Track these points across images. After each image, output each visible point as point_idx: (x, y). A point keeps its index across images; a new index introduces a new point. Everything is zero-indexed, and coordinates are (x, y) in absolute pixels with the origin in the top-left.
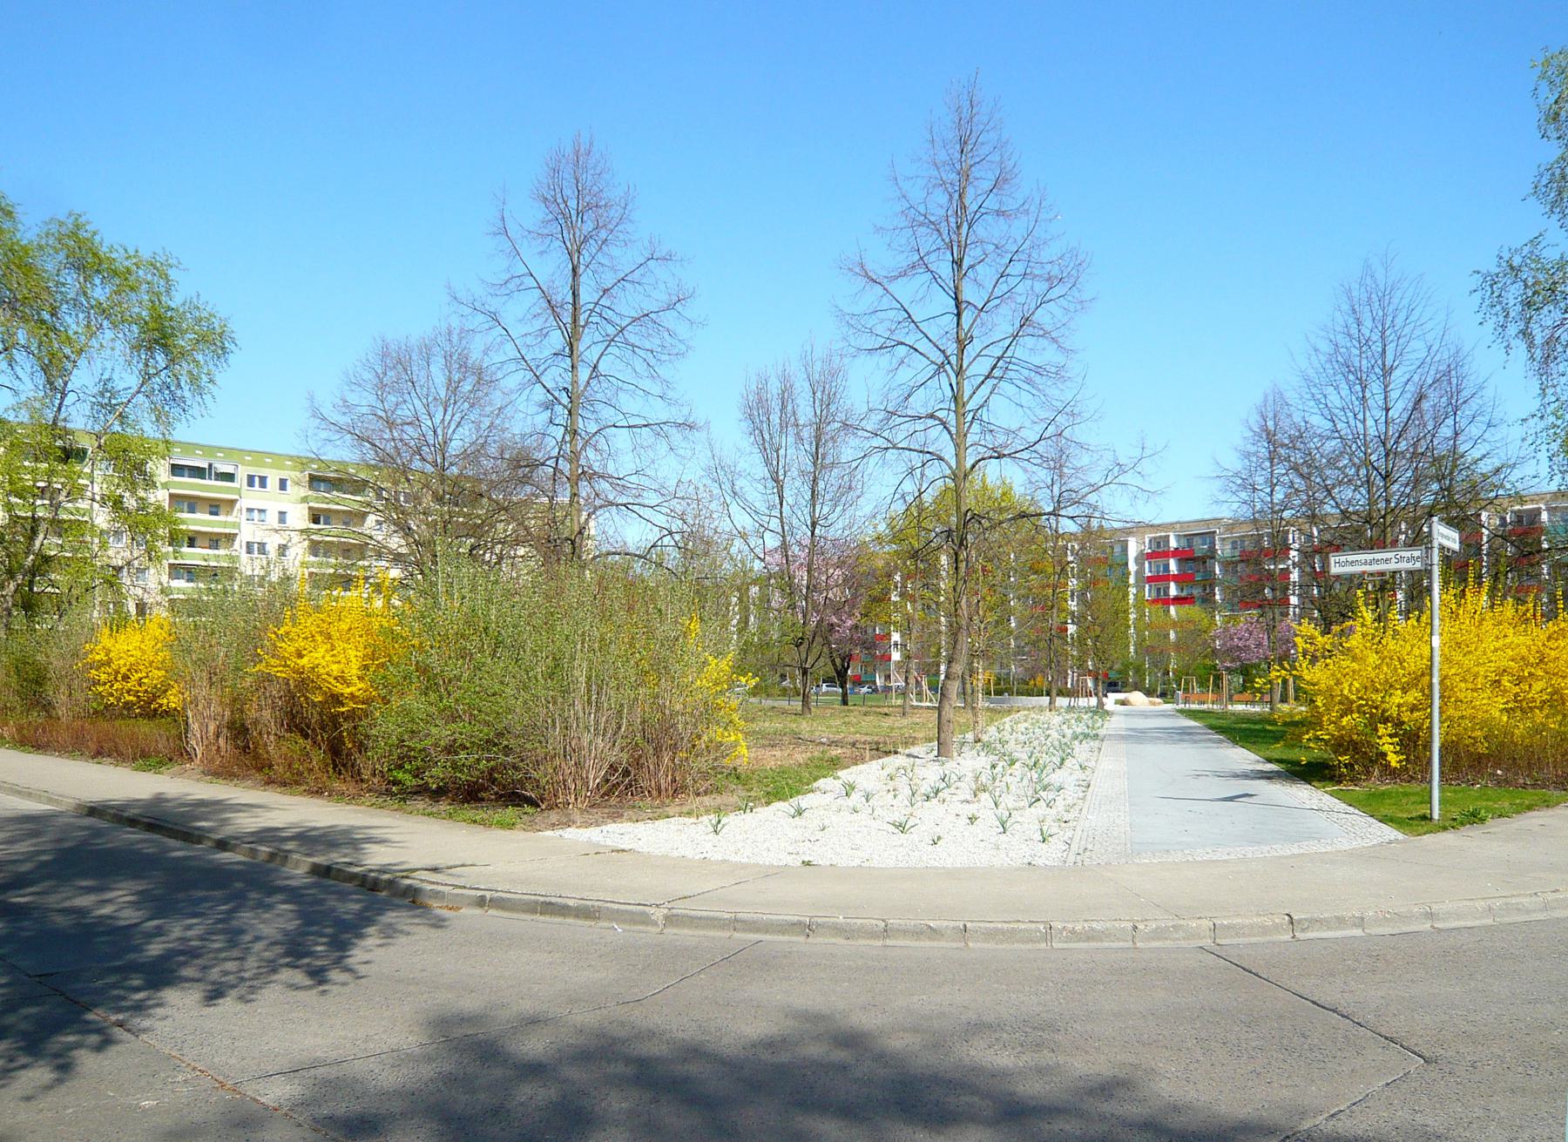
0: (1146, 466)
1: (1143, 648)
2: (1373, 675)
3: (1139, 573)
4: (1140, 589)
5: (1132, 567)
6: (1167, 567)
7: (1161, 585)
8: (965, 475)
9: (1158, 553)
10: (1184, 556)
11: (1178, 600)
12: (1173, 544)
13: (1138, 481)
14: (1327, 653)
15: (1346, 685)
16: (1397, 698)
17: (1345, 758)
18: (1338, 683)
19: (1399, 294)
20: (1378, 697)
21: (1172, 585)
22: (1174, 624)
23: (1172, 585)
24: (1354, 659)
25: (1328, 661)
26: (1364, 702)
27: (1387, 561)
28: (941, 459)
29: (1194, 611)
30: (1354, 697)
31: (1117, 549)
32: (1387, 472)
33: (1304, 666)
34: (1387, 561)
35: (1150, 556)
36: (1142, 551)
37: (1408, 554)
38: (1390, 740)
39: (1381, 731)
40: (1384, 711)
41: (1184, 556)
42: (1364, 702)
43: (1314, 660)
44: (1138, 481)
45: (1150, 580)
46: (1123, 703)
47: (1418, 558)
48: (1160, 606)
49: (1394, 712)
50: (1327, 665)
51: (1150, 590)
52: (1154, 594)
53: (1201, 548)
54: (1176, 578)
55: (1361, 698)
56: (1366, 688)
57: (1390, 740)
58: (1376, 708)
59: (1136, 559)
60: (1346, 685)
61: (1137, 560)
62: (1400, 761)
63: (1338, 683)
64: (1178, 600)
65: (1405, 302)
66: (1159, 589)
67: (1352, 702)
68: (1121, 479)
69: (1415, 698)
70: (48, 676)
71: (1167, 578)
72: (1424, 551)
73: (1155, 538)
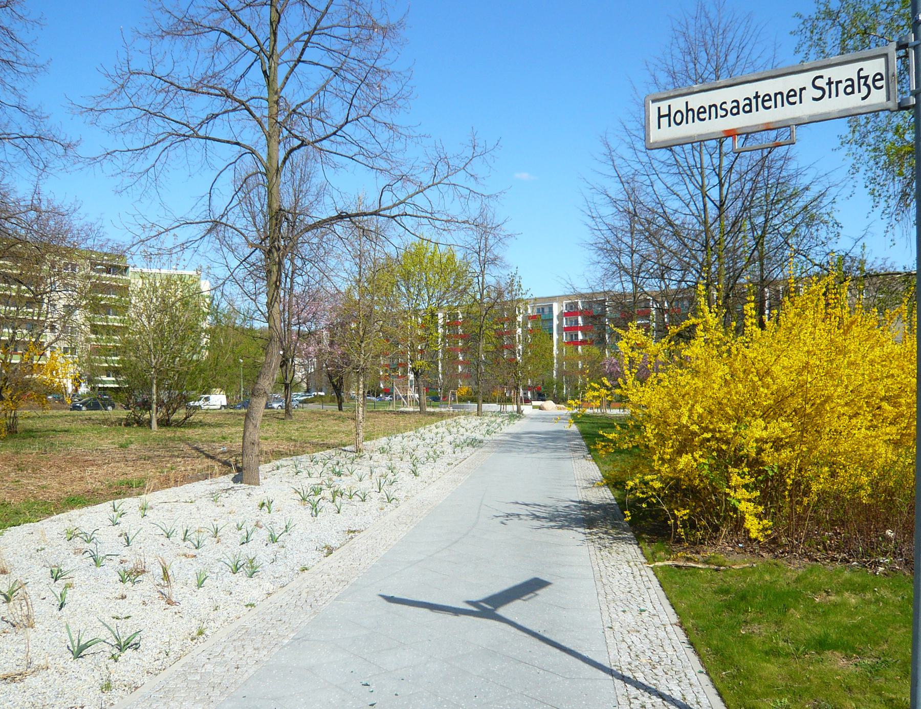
0: (477, 167)
1: (561, 373)
2: (721, 394)
3: (559, 326)
4: (560, 334)
5: (556, 322)
6: (577, 321)
7: (573, 333)
8: (278, 170)
9: (571, 312)
10: (586, 314)
11: (583, 342)
12: (580, 306)
13: (471, 184)
14: (660, 366)
15: (685, 410)
16: (757, 430)
17: (682, 513)
18: (675, 405)
19: (731, 35)
20: (729, 428)
21: (580, 333)
22: (580, 357)
23: (580, 333)
24: (696, 373)
25: (661, 375)
26: (709, 435)
27: (791, 97)
28: (253, 153)
29: (595, 350)
30: (695, 428)
31: (546, 310)
32: (721, 201)
33: (630, 382)
34: (791, 97)
35: (566, 315)
36: (562, 311)
37: (849, 71)
38: (747, 495)
39: (735, 480)
40: (740, 448)
41: (586, 314)
42: (709, 435)
43: (642, 378)
44: (471, 184)
45: (566, 329)
46: (541, 408)
47: (878, 77)
48: (572, 345)
49: (751, 450)
50: (660, 381)
51: (566, 336)
52: (569, 338)
53: (597, 309)
54: (581, 329)
55: (706, 429)
56: (711, 412)
57: (747, 495)
58: (727, 442)
59: (558, 316)
60: (685, 410)
61: (560, 318)
62: (765, 529)
63: (675, 405)
64: (583, 342)
65: (737, 41)
66: (572, 335)
67: (694, 434)
68: (452, 179)
69: (784, 431)
70: (696, 379)
71: (576, 328)
72: (893, 54)
73: (569, 303)
